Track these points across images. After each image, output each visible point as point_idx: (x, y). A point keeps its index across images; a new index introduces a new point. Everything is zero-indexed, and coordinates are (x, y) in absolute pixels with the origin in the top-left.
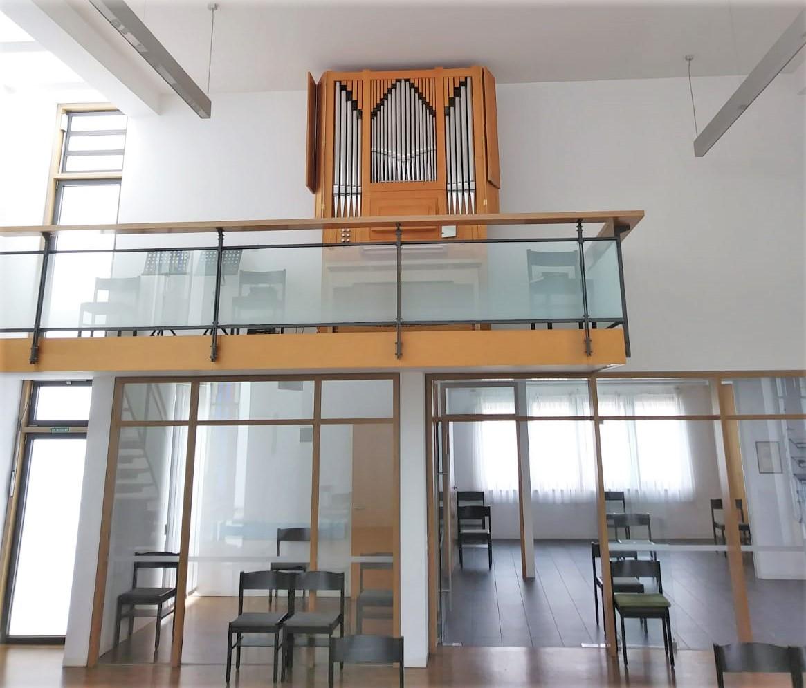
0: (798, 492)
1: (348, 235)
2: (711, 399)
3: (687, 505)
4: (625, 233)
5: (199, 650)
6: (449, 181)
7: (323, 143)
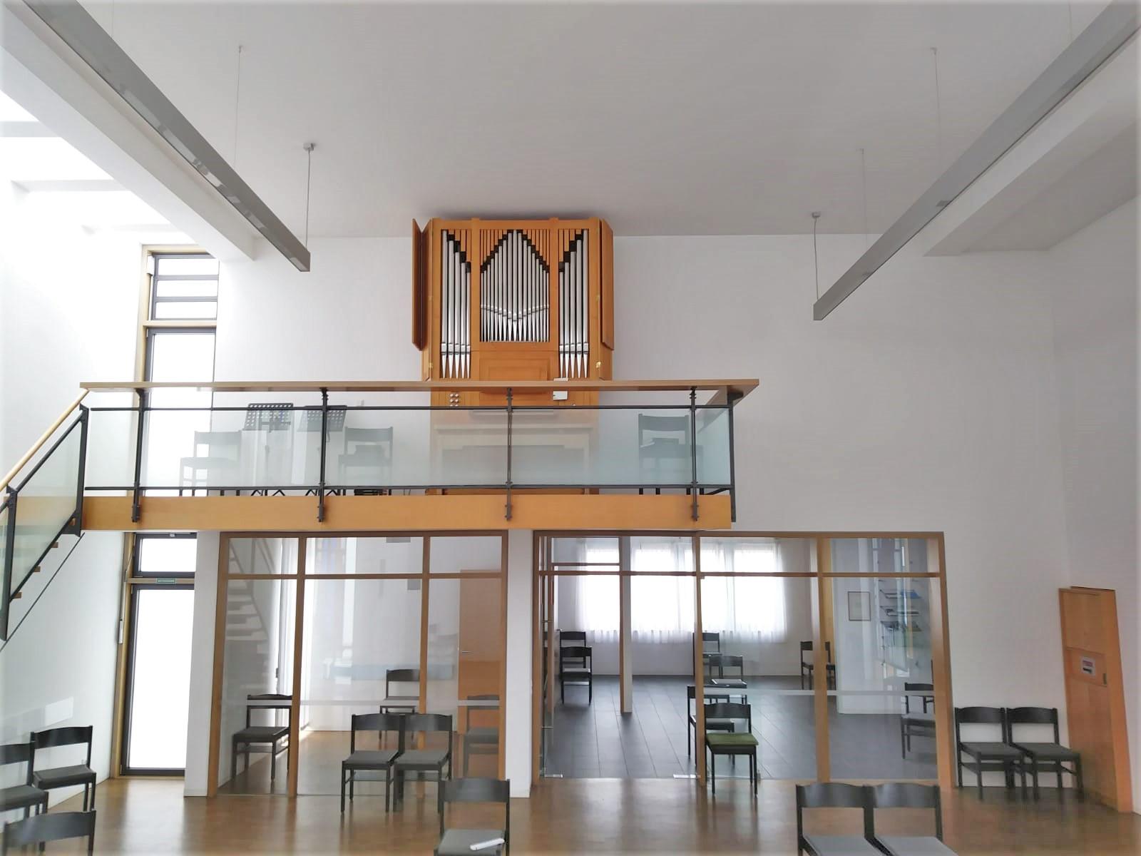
0: (883, 637)
1: (457, 401)
2: (810, 557)
3: (780, 646)
4: (737, 400)
5: (315, 803)
6: (562, 342)
7: (430, 298)
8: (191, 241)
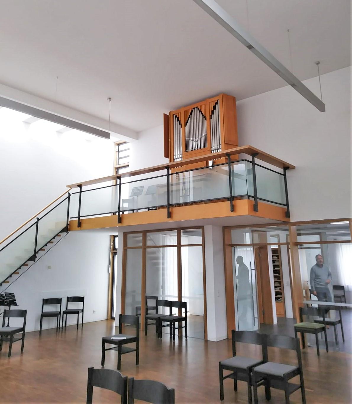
8: (119, 140)
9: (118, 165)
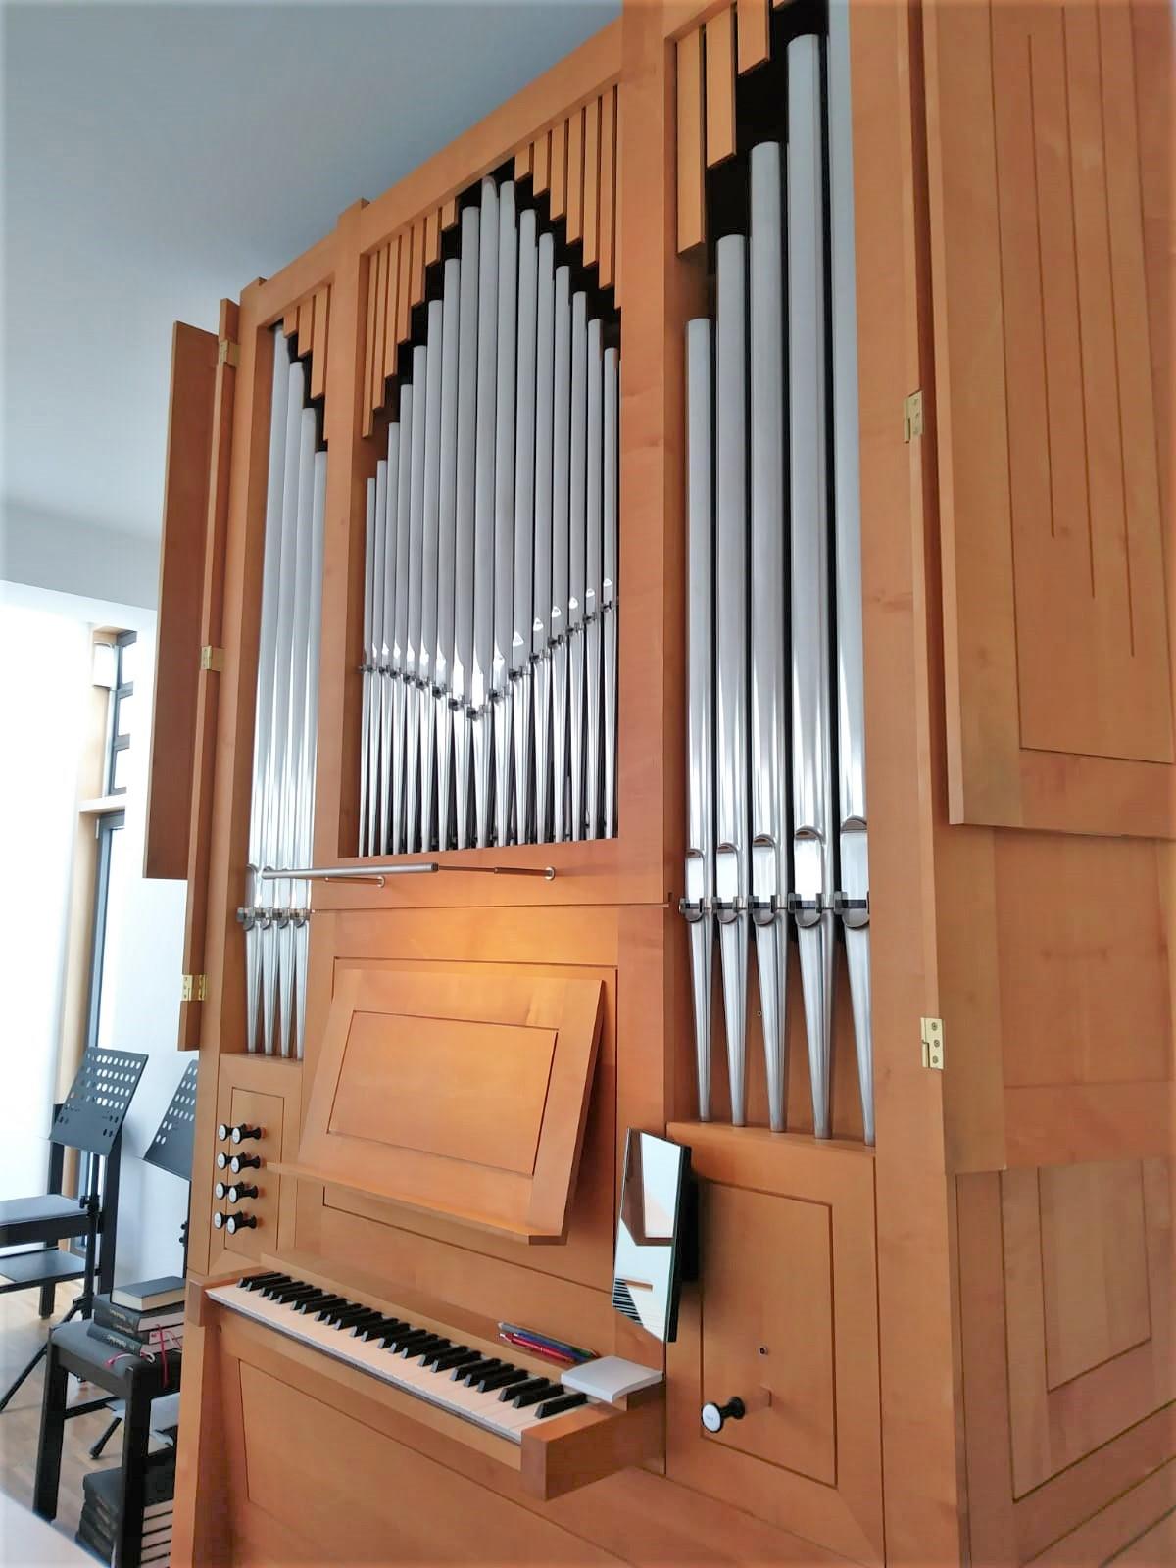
9: (111, 791)
